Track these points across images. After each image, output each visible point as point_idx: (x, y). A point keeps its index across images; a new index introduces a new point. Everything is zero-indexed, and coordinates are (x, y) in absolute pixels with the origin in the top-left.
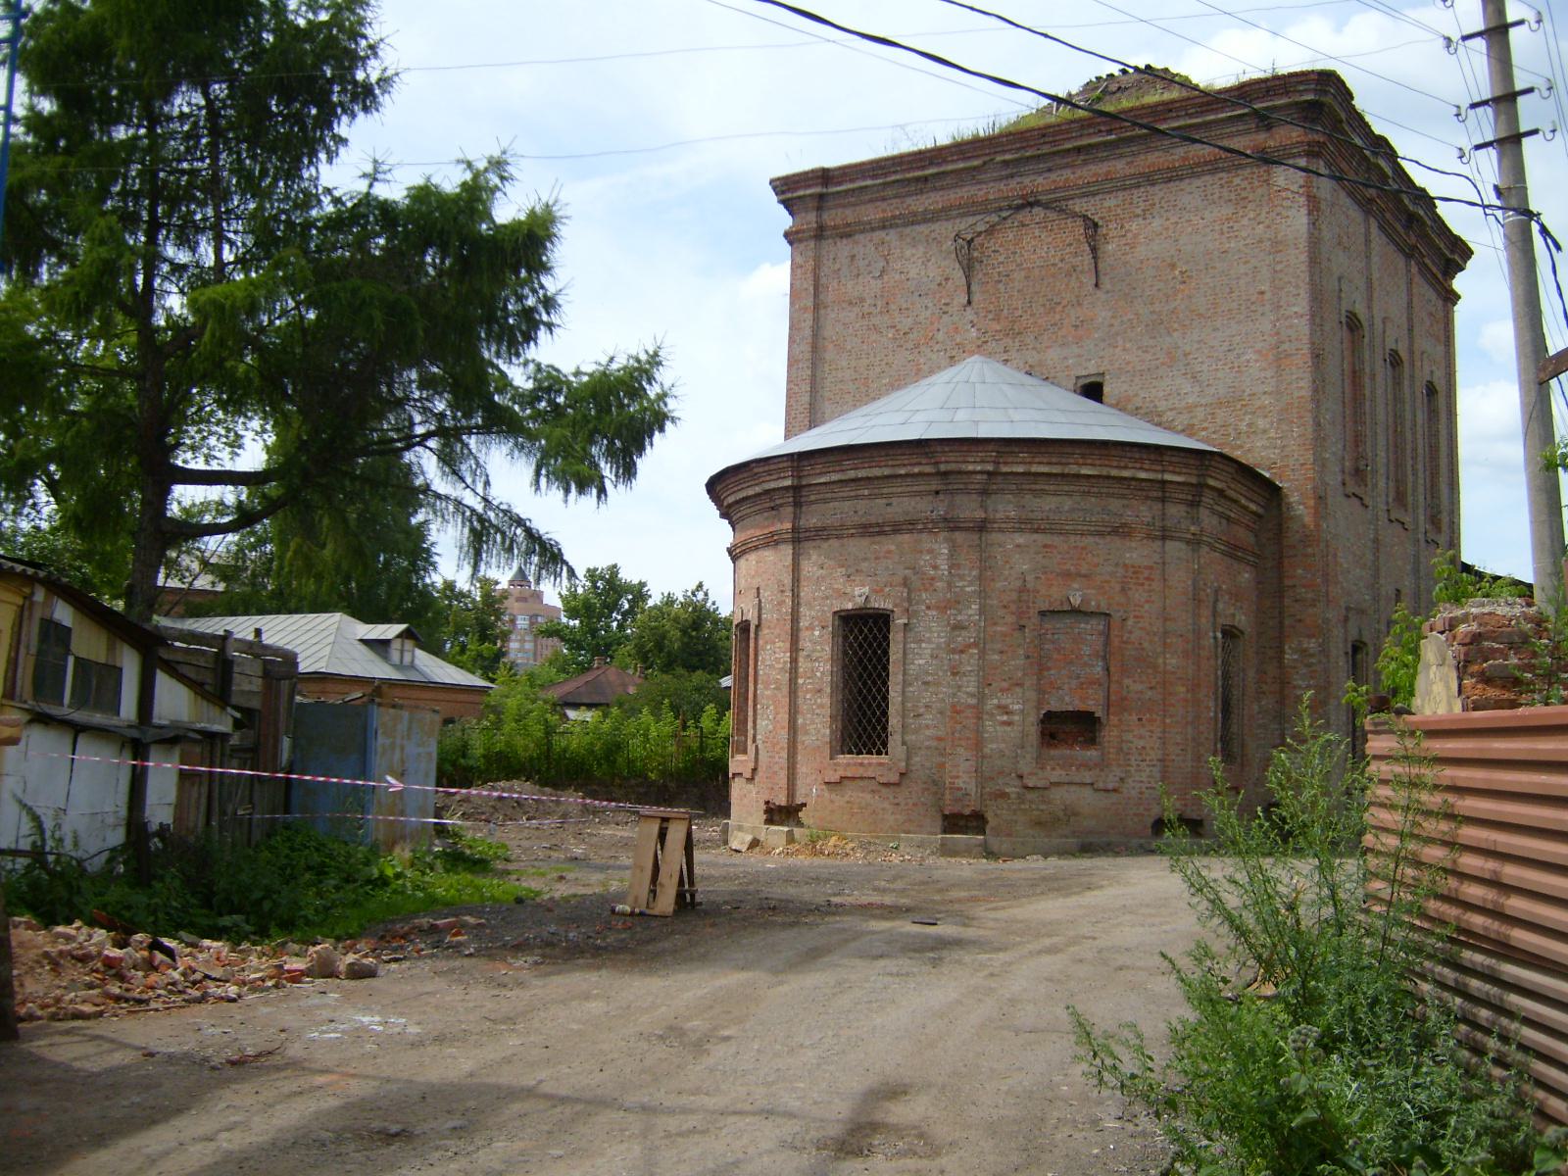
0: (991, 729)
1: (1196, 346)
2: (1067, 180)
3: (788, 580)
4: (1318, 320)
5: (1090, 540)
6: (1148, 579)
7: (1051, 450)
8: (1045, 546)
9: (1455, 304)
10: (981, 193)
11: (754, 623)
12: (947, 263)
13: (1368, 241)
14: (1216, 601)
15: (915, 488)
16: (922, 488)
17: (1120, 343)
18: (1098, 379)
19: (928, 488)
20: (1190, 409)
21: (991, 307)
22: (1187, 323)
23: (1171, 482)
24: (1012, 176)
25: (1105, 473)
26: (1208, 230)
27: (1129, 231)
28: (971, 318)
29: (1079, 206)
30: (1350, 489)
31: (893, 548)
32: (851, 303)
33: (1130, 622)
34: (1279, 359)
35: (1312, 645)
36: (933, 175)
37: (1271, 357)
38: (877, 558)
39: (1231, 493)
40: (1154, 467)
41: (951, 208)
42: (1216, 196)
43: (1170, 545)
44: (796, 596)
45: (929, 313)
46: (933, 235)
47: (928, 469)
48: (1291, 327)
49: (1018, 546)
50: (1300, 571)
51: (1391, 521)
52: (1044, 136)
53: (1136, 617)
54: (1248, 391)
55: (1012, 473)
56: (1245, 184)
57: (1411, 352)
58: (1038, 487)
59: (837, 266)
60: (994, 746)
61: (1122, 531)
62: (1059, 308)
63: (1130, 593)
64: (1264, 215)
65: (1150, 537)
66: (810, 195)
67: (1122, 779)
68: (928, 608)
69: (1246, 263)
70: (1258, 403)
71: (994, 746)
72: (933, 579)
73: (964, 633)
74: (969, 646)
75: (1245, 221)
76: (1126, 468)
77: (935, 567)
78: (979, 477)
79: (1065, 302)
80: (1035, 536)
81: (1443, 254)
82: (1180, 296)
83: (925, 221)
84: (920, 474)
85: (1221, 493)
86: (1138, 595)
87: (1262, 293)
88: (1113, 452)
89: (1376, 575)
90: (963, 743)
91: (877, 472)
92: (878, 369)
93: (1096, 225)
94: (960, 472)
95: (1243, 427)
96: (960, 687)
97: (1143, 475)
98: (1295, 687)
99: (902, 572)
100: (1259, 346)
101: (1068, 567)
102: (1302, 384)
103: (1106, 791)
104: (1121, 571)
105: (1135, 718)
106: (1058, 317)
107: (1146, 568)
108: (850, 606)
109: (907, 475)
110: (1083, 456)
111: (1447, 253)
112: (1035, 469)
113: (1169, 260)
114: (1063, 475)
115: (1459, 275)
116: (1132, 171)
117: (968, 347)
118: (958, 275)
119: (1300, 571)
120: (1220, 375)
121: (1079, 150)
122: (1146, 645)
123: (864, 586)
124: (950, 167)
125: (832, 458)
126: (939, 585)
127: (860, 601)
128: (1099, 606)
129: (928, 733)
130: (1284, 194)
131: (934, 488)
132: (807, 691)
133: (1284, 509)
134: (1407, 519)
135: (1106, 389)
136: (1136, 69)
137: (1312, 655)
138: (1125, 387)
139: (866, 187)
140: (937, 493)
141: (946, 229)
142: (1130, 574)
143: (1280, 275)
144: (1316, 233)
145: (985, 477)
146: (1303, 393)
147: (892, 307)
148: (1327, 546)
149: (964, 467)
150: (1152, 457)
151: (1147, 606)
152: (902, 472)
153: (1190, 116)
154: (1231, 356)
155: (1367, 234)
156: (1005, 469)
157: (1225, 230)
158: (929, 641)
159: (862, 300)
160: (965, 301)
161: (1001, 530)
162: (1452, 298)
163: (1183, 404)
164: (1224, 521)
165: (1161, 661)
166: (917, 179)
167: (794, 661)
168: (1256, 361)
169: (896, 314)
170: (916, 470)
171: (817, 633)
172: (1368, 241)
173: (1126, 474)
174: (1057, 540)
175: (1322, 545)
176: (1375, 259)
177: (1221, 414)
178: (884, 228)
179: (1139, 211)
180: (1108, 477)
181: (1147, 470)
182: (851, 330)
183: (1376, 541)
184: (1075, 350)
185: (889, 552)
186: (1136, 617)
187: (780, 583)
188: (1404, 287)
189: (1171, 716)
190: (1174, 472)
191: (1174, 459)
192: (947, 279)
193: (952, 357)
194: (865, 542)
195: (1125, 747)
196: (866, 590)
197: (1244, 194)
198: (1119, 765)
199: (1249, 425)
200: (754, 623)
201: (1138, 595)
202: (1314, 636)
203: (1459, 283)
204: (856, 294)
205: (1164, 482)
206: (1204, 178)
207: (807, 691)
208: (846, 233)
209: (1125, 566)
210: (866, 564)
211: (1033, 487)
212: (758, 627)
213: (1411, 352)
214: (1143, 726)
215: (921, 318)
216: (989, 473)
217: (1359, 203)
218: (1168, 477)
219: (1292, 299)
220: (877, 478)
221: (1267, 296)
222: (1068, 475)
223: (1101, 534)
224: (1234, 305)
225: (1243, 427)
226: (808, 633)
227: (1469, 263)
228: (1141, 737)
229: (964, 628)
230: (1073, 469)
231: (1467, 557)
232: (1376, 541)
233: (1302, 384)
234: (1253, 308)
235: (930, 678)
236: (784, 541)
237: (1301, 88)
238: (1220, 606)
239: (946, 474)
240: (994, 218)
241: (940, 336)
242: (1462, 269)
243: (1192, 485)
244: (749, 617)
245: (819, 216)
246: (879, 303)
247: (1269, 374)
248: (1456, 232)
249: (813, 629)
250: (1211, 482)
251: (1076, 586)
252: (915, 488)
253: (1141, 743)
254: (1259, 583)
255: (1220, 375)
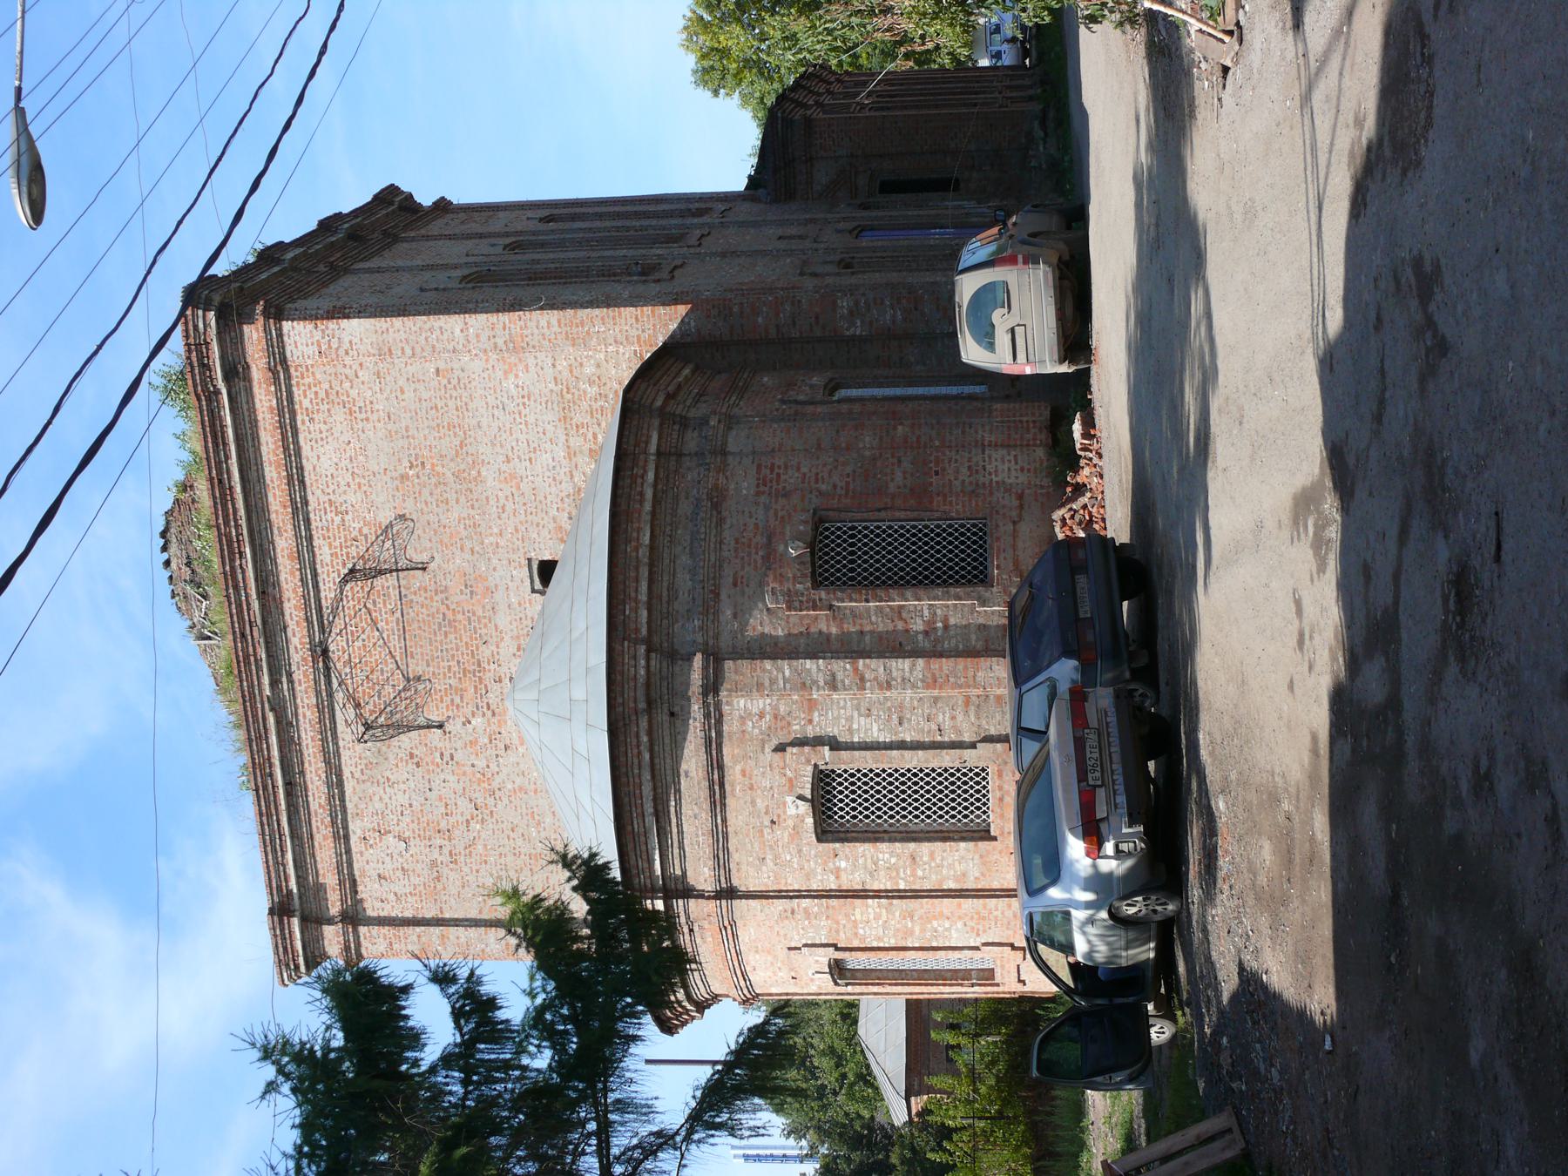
0: (953, 641)
1: (498, 449)
2: (296, 607)
3: (780, 905)
4: (471, 306)
5: (726, 534)
6: (772, 471)
7: (621, 578)
8: (735, 585)
9: (450, 203)
10: (308, 714)
11: (832, 954)
12: (391, 757)
13: (379, 270)
14: (797, 402)
15: (667, 741)
16: (666, 733)
17: (492, 539)
18: (535, 567)
19: (666, 725)
20: (571, 454)
21: (447, 699)
22: (470, 460)
23: (659, 445)
24: (290, 675)
25: (648, 518)
26: (363, 436)
27: (360, 530)
28: (459, 725)
29: (328, 592)
30: (665, 275)
31: (738, 768)
32: (438, 879)
33: (823, 487)
34: (517, 347)
35: (844, 304)
36: (284, 776)
37: (513, 360)
38: (751, 788)
39: (671, 389)
40: (641, 463)
41: (325, 751)
42: (323, 427)
43: (732, 446)
44: (799, 895)
45: (452, 778)
46: (357, 775)
47: (644, 723)
48: (478, 336)
49: (735, 616)
50: (760, 320)
51: (700, 245)
52: (243, 635)
53: (817, 482)
54: (552, 386)
55: (649, 623)
56: (310, 395)
57: (507, 235)
58: (665, 594)
59: (392, 897)
60: (973, 637)
61: (717, 500)
62: (450, 615)
63: (788, 488)
64: (347, 371)
65: (722, 469)
66: (302, 932)
67: (1006, 490)
68: (810, 721)
69: (402, 392)
70: (566, 373)
71: (973, 637)
72: (776, 717)
73: (840, 676)
74: (856, 670)
75: (354, 393)
76: (642, 494)
77: (761, 715)
78: (653, 663)
79: (443, 608)
80: (723, 596)
81: (393, 211)
82: (439, 469)
83: (340, 784)
84: (650, 733)
85: (669, 397)
86: (791, 479)
87: (438, 370)
88: (624, 507)
89: (763, 253)
90: (970, 674)
91: (647, 789)
92: (520, 842)
93: (352, 571)
94: (648, 685)
95: (593, 391)
96: (904, 679)
97: (651, 476)
98: (894, 322)
99: (768, 754)
100: (499, 374)
101: (759, 558)
102: (543, 323)
103: (1021, 507)
104: (763, 499)
105: (934, 479)
106: (460, 617)
107: (759, 472)
108: (810, 821)
109: (651, 751)
110: (628, 541)
111: (392, 208)
112: (643, 597)
113: (397, 482)
114: (651, 565)
115: (418, 199)
116: (290, 527)
117: (495, 728)
118: (406, 741)
119: (760, 320)
120: (531, 419)
121: (262, 594)
122: (849, 469)
123: (785, 804)
124: (275, 753)
125: (630, 846)
126: (782, 709)
127: (804, 808)
128: (805, 522)
129: (960, 718)
130: (324, 348)
131: (666, 718)
132: (914, 874)
133: (689, 340)
134: (698, 233)
135: (547, 557)
136: (164, 549)
137: (857, 303)
138: (545, 532)
139: (295, 861)
140: (672, 714)
141: (352, 755)
142: (766, 489)
143: (418, 350)
144: (369, 309)
145: (653, 655)
146: (554, 322)
147: (443, 825)
148: (731, 290)
149: (641, 681)
150: (629, 464)
151: (804, 470)
152: (647, 756)
153: (227, 457)
154: (511, 407)
155: (370, 271)
156: (644, 631)
157: (363, 416)
158: (850, 719)
159: (434, 863)
160: (439, 731)
161: (717, 637)
162: (442, 206)
163: (564, 462)
164: (703, 399)
165: (867, 453)
166: (288, 794)
167: (877, 894)
168: (516, 376)
169: (452, 820)
170: (645, 739)
171: (843, 864)
172: (379, 270)
173: (649, 493)
174: (728, 572)
175: (730, 295)
176: (400, 263)
177: (578, 418)
178: (347, 837)
179: (338, 519)
180: (653, 513)
181: (645, 471)
182: (471, 878)
183: (723, 255)
184: (498, 596)
185: (743, 773)
186: (817, 482)
187: (783, 916)
188: (432, 243)
189: (931, 440)
190: (647, 443)
191: (632, 442)
192: (412, 756)
193: (506, 748)
194: (730, 802)
195: (969, 489)
196: (789, 799)
197: (322, 394)
198: (991, 494)
199: (591, 383)
200: (832, 954)
201: (791, 479)
202: (834, 303)
203: (425, 199)
204: (426, 872)
205: (659, 453)
206: (302, 443)
207: (914, 874)
208: (350, 883)
209: (758, 494)
210: (759, 801)
211: (665, 599)
212: (837, 949)
213: (507, 235)
214: (944, 469)
215: (459, 788)
216: (649, 651)
217: (333, 280)
218: (653, 448)
219: (445, 336)
220: (655, 789)
221: (442, 365)
222: (651, 558)
223: (721, 521)
224: (451, 404)
225: (593, 391)
226: (843, 876)
227: (405, 188)
228: (957, 471)
229: (833, 675)
230: (643, 553)
231: (738, 184)
232: (723, 255)
233: (543, 323)
234: (454, 382)
235: (895, 717)
236: (731, 911)
237: (201, 325)
238: (801, 397)
239: (650, 702)
240: (339, 696)
241: (481, 764)
242: (411, 196)
243: (661, 425)
244: (825, 961)
245: (330, 922)
246: (438, 842)
247: (531, 361)
248: (369, 199)
249: (838, 869)
250: (659, 403)
251: (781, 548)
252: (667, 741)
253: (964, 471)
254: (775, 369)
255: (531, 419)
